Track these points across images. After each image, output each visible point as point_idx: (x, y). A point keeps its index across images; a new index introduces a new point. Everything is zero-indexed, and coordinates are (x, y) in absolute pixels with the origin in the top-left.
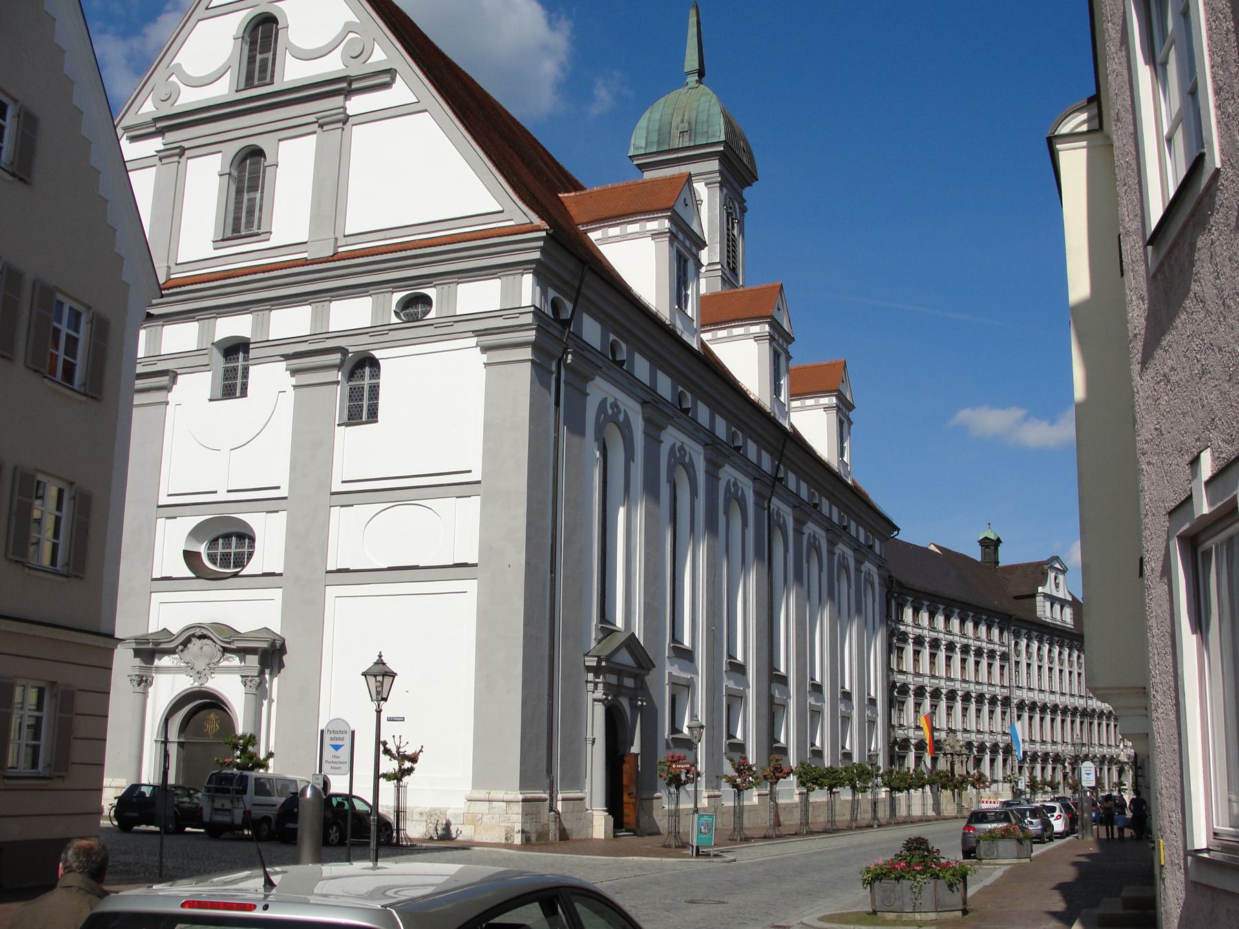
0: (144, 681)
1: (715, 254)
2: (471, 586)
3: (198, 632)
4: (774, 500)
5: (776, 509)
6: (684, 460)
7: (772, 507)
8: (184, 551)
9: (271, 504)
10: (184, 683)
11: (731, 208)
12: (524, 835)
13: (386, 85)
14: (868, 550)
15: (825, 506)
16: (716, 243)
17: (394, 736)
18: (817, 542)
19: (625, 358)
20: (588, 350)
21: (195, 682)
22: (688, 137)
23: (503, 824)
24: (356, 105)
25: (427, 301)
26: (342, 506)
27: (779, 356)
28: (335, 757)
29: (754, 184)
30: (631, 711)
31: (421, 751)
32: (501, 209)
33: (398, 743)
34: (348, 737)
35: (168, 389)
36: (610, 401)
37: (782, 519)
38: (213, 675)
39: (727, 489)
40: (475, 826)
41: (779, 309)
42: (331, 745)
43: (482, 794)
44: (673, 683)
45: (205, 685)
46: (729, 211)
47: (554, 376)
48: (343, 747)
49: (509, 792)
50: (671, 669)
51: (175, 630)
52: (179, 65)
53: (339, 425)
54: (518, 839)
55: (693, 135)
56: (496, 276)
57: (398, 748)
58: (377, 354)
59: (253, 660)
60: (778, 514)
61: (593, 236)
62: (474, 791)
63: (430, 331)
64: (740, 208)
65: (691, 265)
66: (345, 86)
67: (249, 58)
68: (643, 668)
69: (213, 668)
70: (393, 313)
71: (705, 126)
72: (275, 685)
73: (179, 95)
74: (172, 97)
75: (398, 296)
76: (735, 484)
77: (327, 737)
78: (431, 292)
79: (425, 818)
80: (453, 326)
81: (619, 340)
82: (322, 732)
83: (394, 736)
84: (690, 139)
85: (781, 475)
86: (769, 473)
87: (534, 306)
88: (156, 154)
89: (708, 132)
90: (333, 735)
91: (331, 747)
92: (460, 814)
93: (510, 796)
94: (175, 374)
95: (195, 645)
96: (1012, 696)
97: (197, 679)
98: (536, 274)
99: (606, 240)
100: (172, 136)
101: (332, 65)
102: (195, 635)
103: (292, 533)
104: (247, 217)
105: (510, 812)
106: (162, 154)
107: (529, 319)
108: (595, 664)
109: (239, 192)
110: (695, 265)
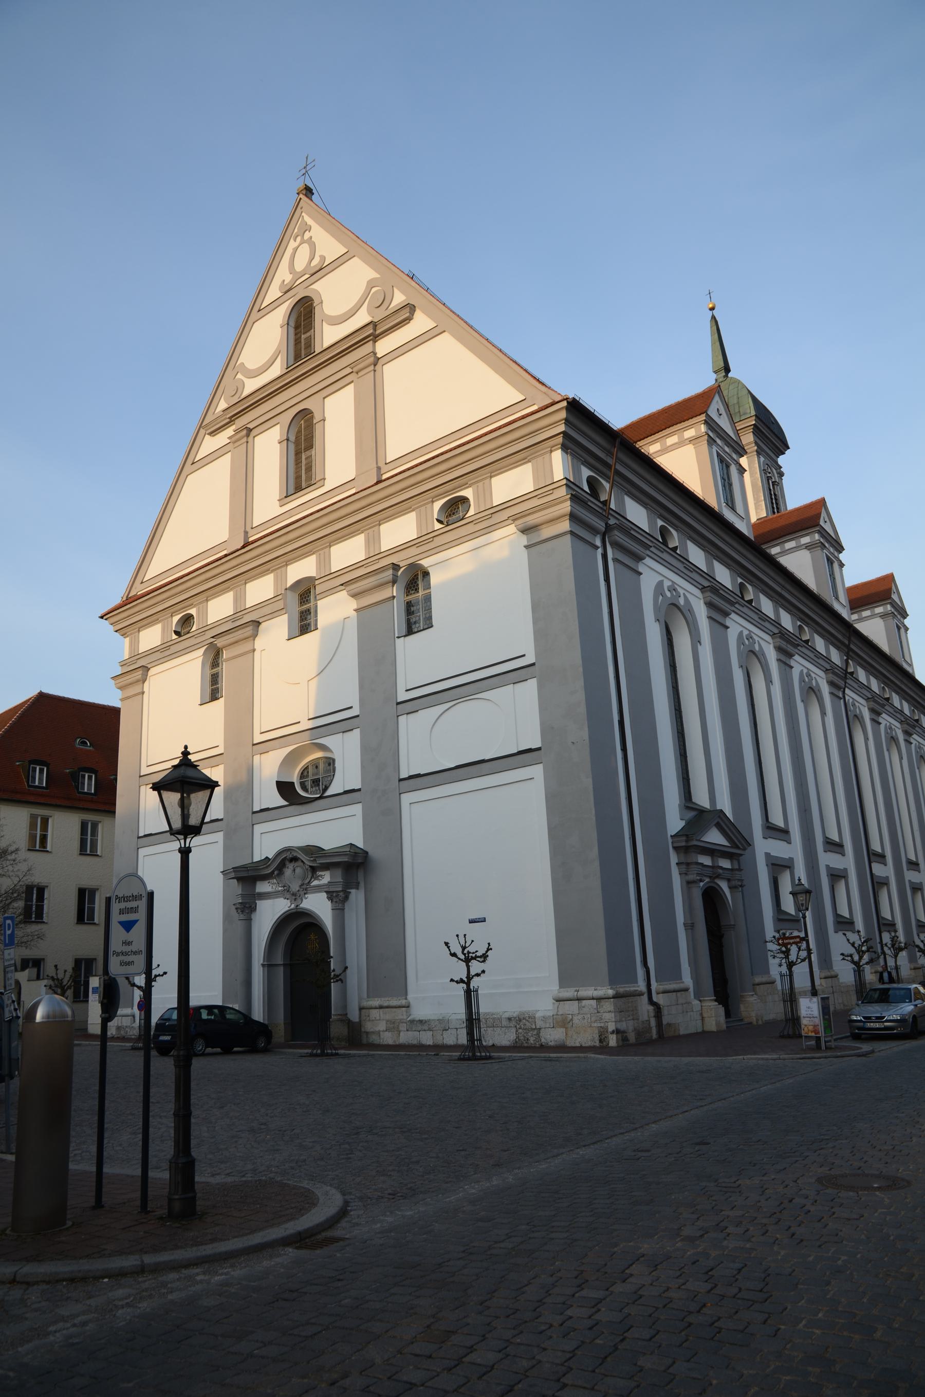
1: (762, 510)
2: (537, 771)
4: (847, 691)
5: (851, 700)
6: (754, 647)
7: (847, 698)
8: (277, 782)
11: (769, 473)
12: (620, 1036)
13: (408, 320)
15: (896, 700)
16: (761, 501)
17: (457, 936)
18: (894, 732)
19: (678, 544)
21: (291, 904)
23: (595, 1025)
24: (383, 346)
25: (464, 500)
26: (407, 714)
27: (728, 466)
28: (127, 943)
29: (786, 452)
30: (731, 892)
31: (488, 950)
32: (524, 398)
33: (463, 943)
34: (142, 904)
35: (255, 635)
36: (667, 583)
37: (857, 709)
38: (306, 896)
39: (802, 680)
40: (566, 1028)
41: (826, 522)
42: (138, 920)
43: (569, 993)
44: (773, 864)
45: (301, 906)
46: (769, 475)
47: (600, 551)
48: (138, 922)
49: (599, 988)
53: (398, 637)
54: (613, 1041)
56: (526, 460)
57: (464, 948)
58: (425, 563)
59: (338, 876)
60: (854, 705)
62: (561, 989)
63: (471, 528)
64: (778, 473)
65: (733, 469)
67: (296, 340)
68: (738, 848)
69: (306, 889)
70: (435, 521)
71: (737, 407)
72: (357, 897)
73: (244, 388)
74: (239, 390)
75: (438, 505)
76: (808, 675)
77: (116, 907)
78: (468, 493)
79: (513, 1023)
82: (108, 900)
83: (457, 936)
85: (850, 670)
87: (566, 478)
88: (229, 441)
89: (739, 412)
90: (123, 905)
91: (119, 925)
92: (549, 1016)
93: (600, 993)
94: (258, 624)
95: (290, 867)
97: (293, 901)
98: (564, 448)
100: (241, 422)
101: (362, 318)
103: (366, 749)
104: (306, 473)
105: (601, 1010)
106: (234, 439)
107: (563, 491)
109: (298, 454)
110: (738, 469)
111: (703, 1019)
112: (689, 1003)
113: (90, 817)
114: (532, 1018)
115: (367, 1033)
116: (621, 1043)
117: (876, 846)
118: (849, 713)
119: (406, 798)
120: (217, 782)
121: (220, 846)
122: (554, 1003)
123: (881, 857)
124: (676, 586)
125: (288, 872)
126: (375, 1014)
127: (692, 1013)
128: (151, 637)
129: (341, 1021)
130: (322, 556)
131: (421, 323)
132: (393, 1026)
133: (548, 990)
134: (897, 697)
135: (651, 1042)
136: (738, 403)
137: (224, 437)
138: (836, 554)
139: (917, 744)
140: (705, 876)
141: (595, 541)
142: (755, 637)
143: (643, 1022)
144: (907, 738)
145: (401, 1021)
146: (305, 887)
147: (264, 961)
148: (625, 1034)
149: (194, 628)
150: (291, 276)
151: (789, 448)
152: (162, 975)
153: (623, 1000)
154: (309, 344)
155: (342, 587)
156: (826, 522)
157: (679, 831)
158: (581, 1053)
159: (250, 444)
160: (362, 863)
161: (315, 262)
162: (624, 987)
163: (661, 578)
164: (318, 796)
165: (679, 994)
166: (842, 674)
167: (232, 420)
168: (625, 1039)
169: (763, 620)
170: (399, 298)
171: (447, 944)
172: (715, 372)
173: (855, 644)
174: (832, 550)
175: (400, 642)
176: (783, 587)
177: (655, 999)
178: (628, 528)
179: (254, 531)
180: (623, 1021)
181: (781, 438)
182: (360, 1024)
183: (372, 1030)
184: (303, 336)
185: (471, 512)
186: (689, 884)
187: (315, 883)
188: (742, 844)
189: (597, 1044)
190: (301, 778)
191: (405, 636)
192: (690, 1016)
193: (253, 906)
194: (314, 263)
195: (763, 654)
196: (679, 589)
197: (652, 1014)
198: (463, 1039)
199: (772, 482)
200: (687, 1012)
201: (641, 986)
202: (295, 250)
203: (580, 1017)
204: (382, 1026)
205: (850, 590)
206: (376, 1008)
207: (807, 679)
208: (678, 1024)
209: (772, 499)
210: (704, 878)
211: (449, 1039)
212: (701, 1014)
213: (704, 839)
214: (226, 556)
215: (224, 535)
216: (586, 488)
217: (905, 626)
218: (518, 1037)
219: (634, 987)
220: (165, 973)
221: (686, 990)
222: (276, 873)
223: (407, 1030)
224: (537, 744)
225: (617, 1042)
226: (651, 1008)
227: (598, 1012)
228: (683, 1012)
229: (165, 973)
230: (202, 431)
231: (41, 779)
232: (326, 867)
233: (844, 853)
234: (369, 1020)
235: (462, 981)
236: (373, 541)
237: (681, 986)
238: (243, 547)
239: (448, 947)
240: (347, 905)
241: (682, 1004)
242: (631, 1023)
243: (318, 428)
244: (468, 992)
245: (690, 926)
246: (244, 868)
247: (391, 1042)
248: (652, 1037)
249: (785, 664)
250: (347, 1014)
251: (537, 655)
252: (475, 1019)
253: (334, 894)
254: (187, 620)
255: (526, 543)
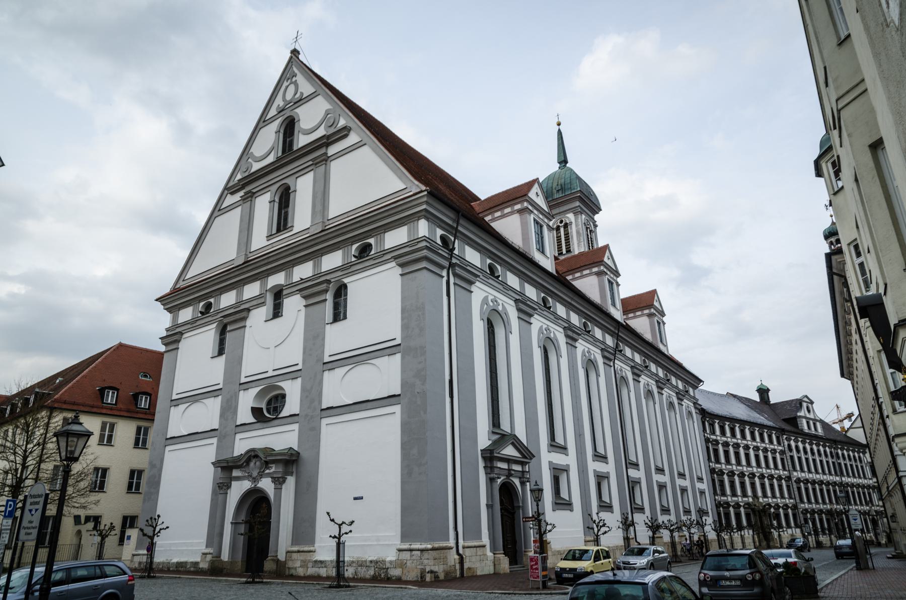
0: (637, 381)
2: (397, 409)
3: (253, 454)
4: (616, 361)
7: (616, 366)
8: (252, 408)
9: (292, 374)
10: (247, 485)
13: (346, 136)
14: (686, 393)
18: (650, 387)
20: (469, 266)
22: (561, 191)
23: (419, 567)
24: (332, 150)
25: (370, 245)
27: (541, 226)
32: (405, 187)
36: (490, 297)
37: (624, 373)
41: (609, 259)
43: (406, 546)
47: (445, 279)
50: (547, 458)
51: (243, 453)
52: (252, 153)
53: (327, 324)
55: (564, 190)
58: (346, 281)
60: (621, 370)
61: (487, 219)
62: (402, 544)
63: (372, 262)
66: (327, 141)
68: (526, 458)
69: (261, 475)
72: (291, 481)
77: (29, 501)
78: (372, 241)
80: (385, 256)
81: (494, 263)
84: (562, 192)
86: (612, 346)
90: (33, 500)
96: (792, 476)
99: (494, 220)
101: (321, 132)
102: (252, 455)
103: (304, 389)
108: (489, 455)
111: (495, 565)
112: (485, 555)
113: (143, 424)
114: (384, 562)
115: (289, 568)
116: (433, 579)
117: (633, 458)
118: (617, 375)
119: (325, 421)
120: (93, 433)
121: (296, 433)
122: (396, 553)
123: (636, 465)
124: (497, 299)
125: (252, 464)
126: (295, 556)
127: (487, 561)
128: (186, 314)
129: (273, 560)
130: (288, 272)
131: (353, 138)
132: (304, 564)
133: (392, 544)
134: (654, 365)
135: (454, 579)
136: (570, 182)
137: (237, 197)
138: (615, 278)
139: (668, 394)
140: (502, 475)
141: (442, 273)
142: (551, 329)
143: (450, 566)
144: (660, 391)
145: (309, 561)
146: (260, 473)
147: (232, 520)
148: (437, 574)
149: (212, 311)
150: (283, 103)
151: (601, 210)
152: (165, 529)
153: (437, 551)
154: (291, 144)
155: (298, 292)
156: (609, 259)
157: (487, 447)
158: (404, 585)
159: (253, 201)
160: (296, 460)
161: (298, 95)
162: (439, 544)
163: (487, 294)
164: (275, 417)
165: (478, 549)
166: (613, 352)
167: (243, 187)
168: (437, 577)
169: (557, 319)
170: (342, 123)
171: (328, 513)
172: (559, 163)
173: (622, 333)
174: (612, 276)
175: (328, 327)
176: (572, 299)
177: (461, 551)
178: (465, 265)
179: (252, 254)
180: (436, 565)
181: (596, 204)
182: (285, 562)
183: (292, 566)
184: (288, 139)
185: (373, 252)
186: (491, 481)
187: (267, 471)
188: (529, 456)
189: (419, 579)
190: (267, 405)
191: (331, 323)
192: (486, 563)
193: (229, 485)
194: (298, 95)
195: (557, 340)
196: (499, 301)
197: (457, 561)
198: (333, 573)
199: (590, 231)
200: (483, 560)
201: (452, 543)
202: (287, 87)
203: (411, 562)
204: (298, 564)
205: (624, 302)
206: (295, 552)
207: (587, 355)
208: (477, 568)
209: (588, 241)
210: (501, 476)
211: (323, 572)
212: (494, 562)
213: (502, 452)
214: (233, 268)
215: (234, 256)
216: (439, 241)
217: (663, 322)
218: (375, 573)
219: (447, 543)
220: (168, 527)
221: (484, 546)
222: (244, 464)
223: (312, 567)
224: (398, 392)
225: (431, 578)
226: (457, 557)
227: (421, 559)
228: (480, 560)
229: (168, 527)
230: (226, 192)
231: (112, 400)
232: (274, 462)
233: (608, 461)
234: (291, 560)
235: (335, 537)
236: (317, 266)
237: (481, 544)
238: (243, 264)
239: (329, 516)
240: (284, 486)
241: (480, 555)
242: (442, 567)
243: (292, 196)
244: (338, 544)
245: (490, 506)
246: (226, 461)
247: (302, 574)
248: (456, 576)
249: (571, 345)
250: (277, 556)
251: (403, 339)
252: (342, 561)
253: (276, 479)
254: (208, 306)
255: (401, 273)
